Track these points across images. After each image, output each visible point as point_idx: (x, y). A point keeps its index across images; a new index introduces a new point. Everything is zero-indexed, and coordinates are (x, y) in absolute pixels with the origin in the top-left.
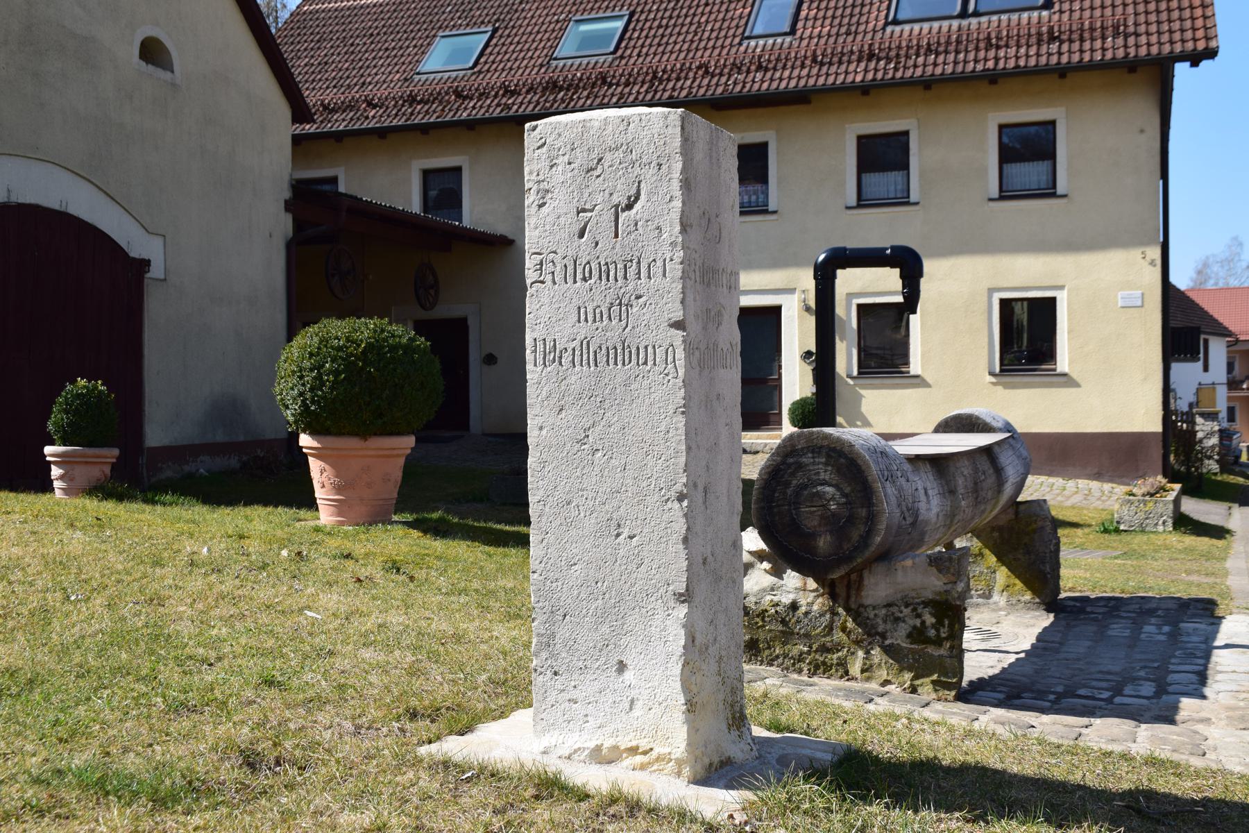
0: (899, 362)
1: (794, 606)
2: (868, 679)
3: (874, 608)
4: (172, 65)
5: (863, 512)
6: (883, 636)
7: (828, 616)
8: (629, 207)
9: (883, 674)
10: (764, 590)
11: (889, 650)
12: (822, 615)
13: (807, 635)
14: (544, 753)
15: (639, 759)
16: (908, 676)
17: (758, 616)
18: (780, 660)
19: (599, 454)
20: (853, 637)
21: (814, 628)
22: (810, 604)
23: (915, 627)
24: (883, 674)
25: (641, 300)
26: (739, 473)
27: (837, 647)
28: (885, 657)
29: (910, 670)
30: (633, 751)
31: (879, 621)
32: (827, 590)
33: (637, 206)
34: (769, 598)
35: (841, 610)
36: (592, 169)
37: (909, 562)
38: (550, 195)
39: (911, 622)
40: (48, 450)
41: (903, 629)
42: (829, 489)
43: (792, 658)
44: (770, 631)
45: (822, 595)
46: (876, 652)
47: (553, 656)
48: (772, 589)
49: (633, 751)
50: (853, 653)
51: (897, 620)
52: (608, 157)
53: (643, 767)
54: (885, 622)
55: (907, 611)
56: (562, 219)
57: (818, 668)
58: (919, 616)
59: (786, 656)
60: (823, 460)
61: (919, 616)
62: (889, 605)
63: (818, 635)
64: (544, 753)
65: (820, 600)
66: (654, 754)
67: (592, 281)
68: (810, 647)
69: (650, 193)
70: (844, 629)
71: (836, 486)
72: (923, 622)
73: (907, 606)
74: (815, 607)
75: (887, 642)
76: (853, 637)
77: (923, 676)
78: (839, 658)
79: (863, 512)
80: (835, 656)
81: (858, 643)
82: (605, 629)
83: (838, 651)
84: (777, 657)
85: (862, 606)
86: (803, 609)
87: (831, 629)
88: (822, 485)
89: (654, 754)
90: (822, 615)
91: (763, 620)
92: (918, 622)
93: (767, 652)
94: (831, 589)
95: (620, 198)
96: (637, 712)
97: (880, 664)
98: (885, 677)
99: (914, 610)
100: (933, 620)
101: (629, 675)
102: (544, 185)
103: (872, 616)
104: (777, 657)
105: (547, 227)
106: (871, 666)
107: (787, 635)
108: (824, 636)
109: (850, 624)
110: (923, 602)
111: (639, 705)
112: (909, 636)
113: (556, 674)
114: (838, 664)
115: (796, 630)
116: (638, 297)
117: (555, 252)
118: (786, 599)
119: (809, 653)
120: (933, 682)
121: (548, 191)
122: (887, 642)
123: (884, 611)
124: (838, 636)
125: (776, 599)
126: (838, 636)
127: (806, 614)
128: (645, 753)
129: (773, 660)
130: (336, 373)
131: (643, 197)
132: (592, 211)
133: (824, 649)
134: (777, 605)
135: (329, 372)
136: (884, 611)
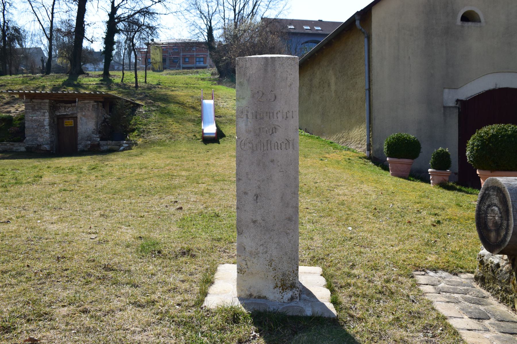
0: (38, 60)
4: (480, 19)
7: (508, 274)
12: (506, 273)
18: (491, 290)
26: (237, 91)
32: (511, 262)
40: (430, 170)
42: (496, 209)
45: (509, 263)
65: (508, 266)
71: (499, 209)
80: (510, 296)
87: (509, 282)
90: (506, 273)
93: (487, 285)
119: (501, 290)
127: (501, 270)
130: (478, 146)
135: (476, 146)
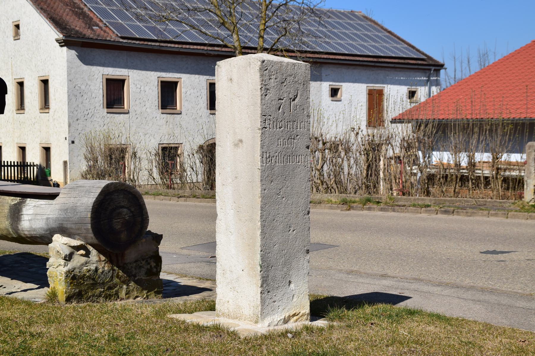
1: (97, 269)
2: (128, 298)
3: (130, 264)
5: (139, 219)
6: (135, 276)
8: (294, 100)
9: (135, 293)
10: (82, 265)
11: (136, 282)
12: (109, 272)
13: (103, 283)
14: (269, 326)
15: (295, 318)
16: (145, 292)
17: (81, 279)
19: (284, 199)
20: (122, 279)
21: (106, 279)
22: (103, 267)
23: (148, 269)
24: (135, 293)
25: (298, 137)
27: (115, 286)
28: (136, 286)
29: (146, 290)
30: (294, 315)
31: (133, 269)
33: (297, 100)
34: (85, 268)
35: (115, 268)
36: (283, 83)
37: (144, 240)
38: (268, 91)
39: (146, 267)
41: (143, 271)
43: (96, 296)
44: (87, 284)
46: (132, 284)
47: (268, 285)
48: (86, 263)
49: (294, 315)
50: (121, 287)
51: (140, 267)
52: (288, 78)
53: (296, 321)
54: (135, 269)
55: (144, 262)
56: (273, 102)
57: (108, 297)
58: (149, 264)
59: (93, 296)
60: (122, 196)
61: (149, 264)
62: (136, 261)
63: (108, 281)
64: (269, 326)
65: (106, 265)
66: (300, 314)
67: (282, 129)
68: (104, 289)
69: (301, 95)
70: (118, 276)
72: (151, 266)
73: (143, 260)
74: (106, 268)
75: (136, 279)
76: (122, 279)
77: (151, 291)
78: (116, 291)
79: (139, 219)
80: (114, 290)
81: (124, 282)
82: (285, 269)
83: (115, 287)
84: (90, 297)
85: (125, 264)
86: (101, 270)
88: (121, 208)
89: (300, 314)
90: (109, 272)
91: (84, 280)
92: (149, 267)
94: (110, 260)
95: (291, 96)
96: (295, 300)
97: (133, 290)
98: (136, 295)
99: (147, 261)
100: (155, 264)
101: (292, 285)
102: (267, 87)
103: (130, 268)
104: (90, 297)
105: (268, 105)
106: (129, 291)
107: (94, 285)
108: (110, 282)
109: (121, 273)
110: (149, 257)
111: (295, 296)
112: (146, 273)
113: (269, 292)
114: (115, 294)
115: (99, 282)
116: (297, 136)
117: (270, 116)
118: (93, 267)
120: (155, 292)
121: (268, 89)
122: (136, 279)
123: (135, 265)
124: (116, 280)
125: (88, 268)
126: (116, 280)
127: (103, 272)
128: (298, 314)
129: (88, 299)
131: (299, 96)
132: (283, 100)
133: (110, 288)
134: (90, 271)
136: (135, 265)
